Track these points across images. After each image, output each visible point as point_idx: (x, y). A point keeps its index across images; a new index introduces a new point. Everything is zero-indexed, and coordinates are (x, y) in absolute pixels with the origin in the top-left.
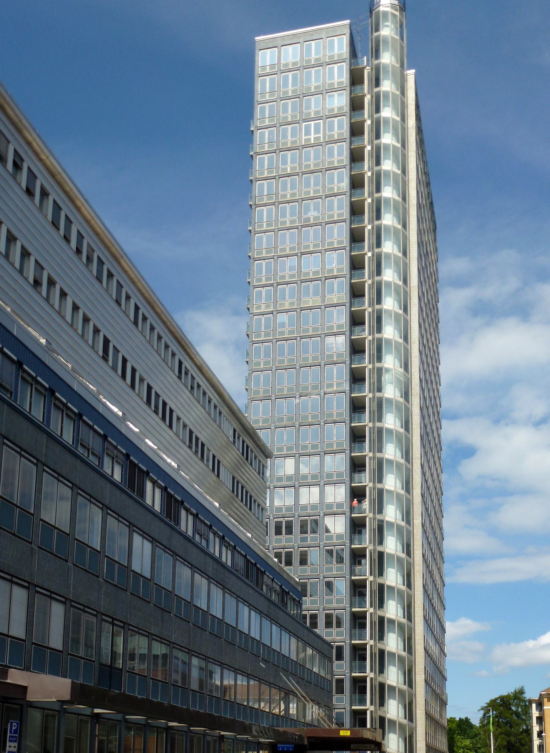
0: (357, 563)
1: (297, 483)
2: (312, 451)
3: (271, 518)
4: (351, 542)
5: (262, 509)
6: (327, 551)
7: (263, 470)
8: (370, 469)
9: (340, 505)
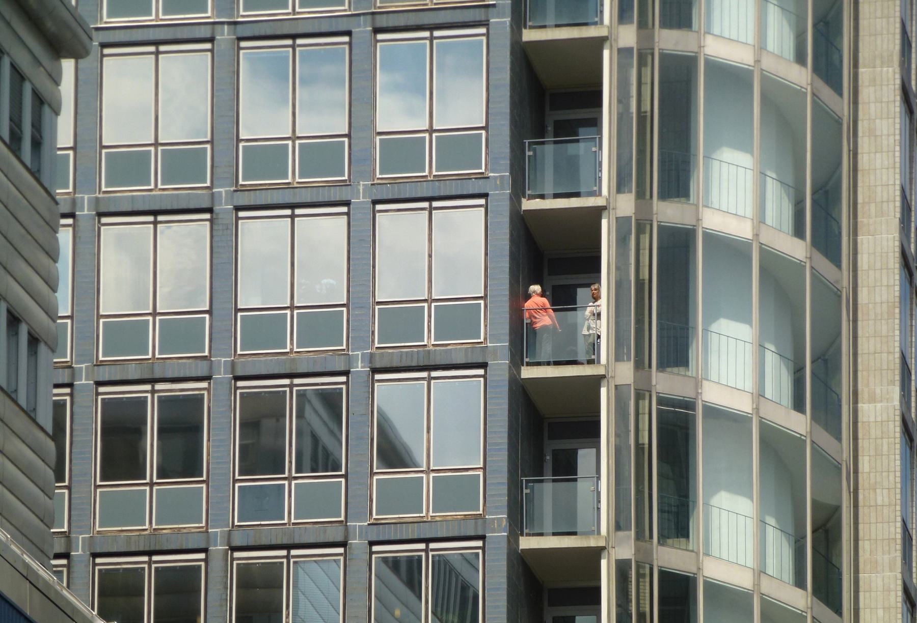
0: (548, 467)
1: (218, 187)
2: (306, 12)
3: (83, 381)
4: (519, 518)
5: (34, 341)
6: (394, 564)
7: (37, 126)
8: (622, 118)
9: (455, 316)
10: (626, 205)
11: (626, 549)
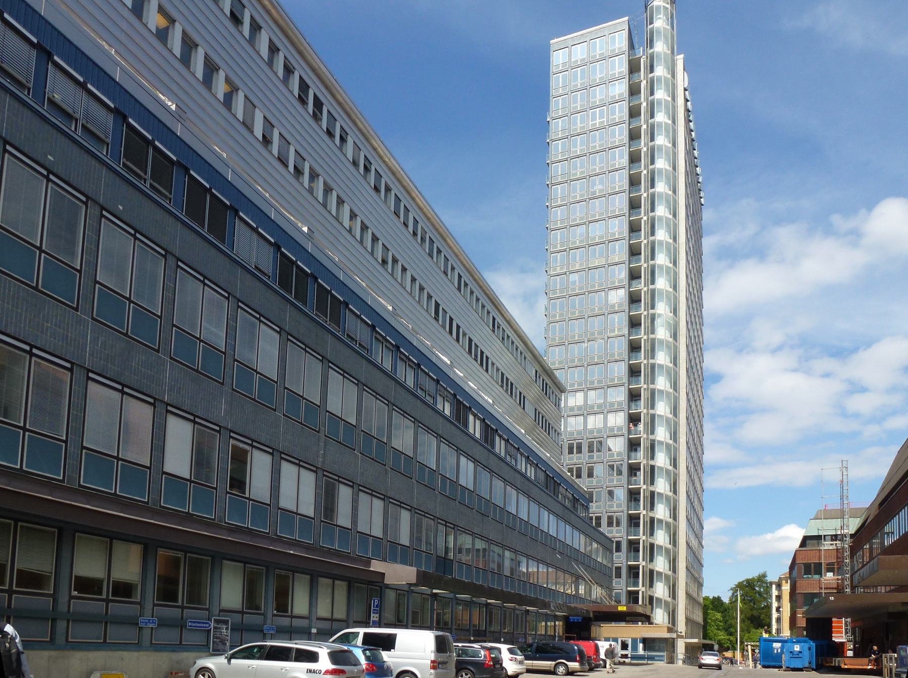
1: (585, 411)
4: (629, 459)
9: (620, 429)
10: (645, 411)
11: (645, 462)
